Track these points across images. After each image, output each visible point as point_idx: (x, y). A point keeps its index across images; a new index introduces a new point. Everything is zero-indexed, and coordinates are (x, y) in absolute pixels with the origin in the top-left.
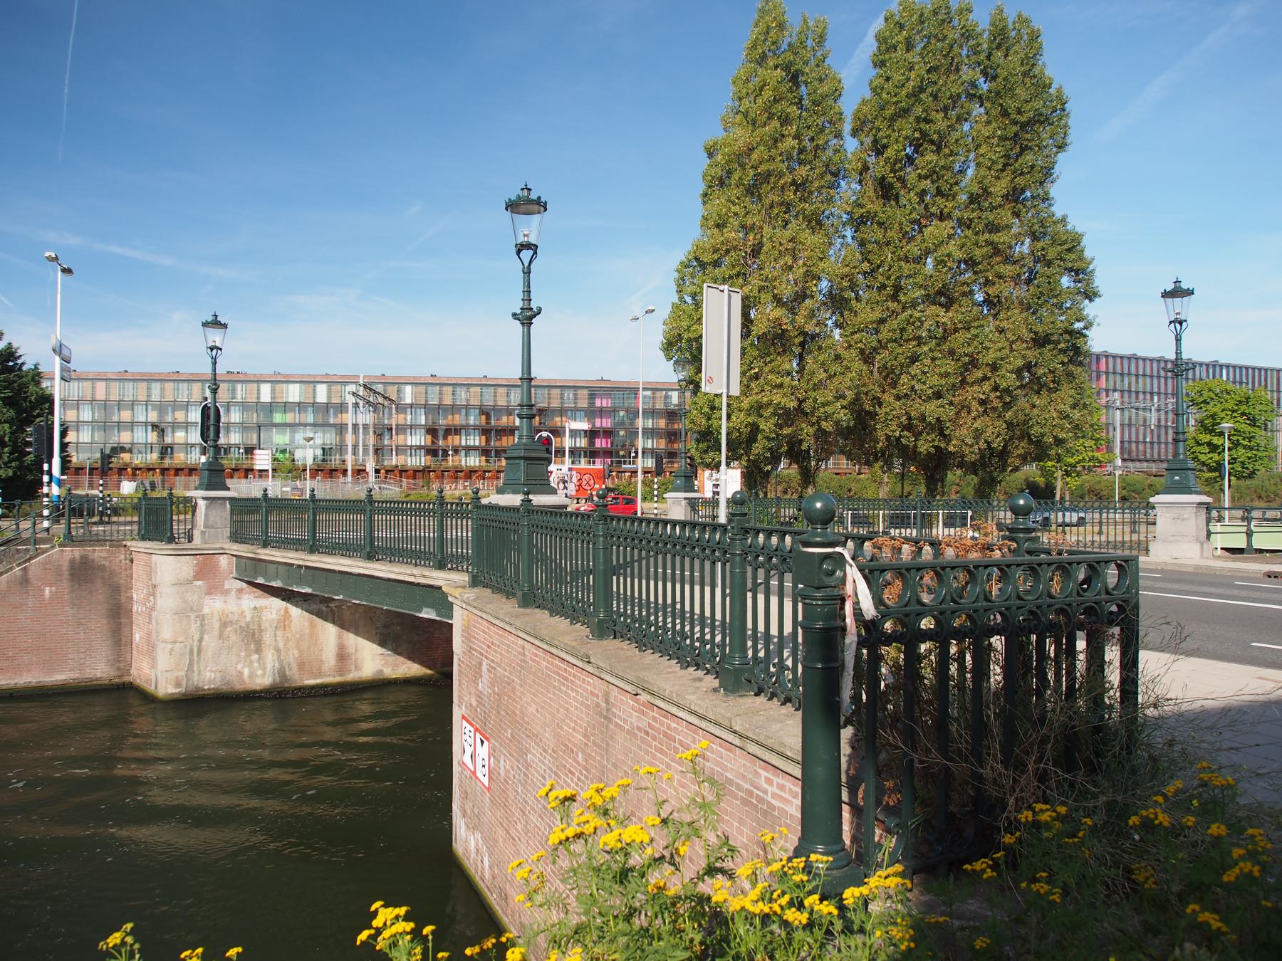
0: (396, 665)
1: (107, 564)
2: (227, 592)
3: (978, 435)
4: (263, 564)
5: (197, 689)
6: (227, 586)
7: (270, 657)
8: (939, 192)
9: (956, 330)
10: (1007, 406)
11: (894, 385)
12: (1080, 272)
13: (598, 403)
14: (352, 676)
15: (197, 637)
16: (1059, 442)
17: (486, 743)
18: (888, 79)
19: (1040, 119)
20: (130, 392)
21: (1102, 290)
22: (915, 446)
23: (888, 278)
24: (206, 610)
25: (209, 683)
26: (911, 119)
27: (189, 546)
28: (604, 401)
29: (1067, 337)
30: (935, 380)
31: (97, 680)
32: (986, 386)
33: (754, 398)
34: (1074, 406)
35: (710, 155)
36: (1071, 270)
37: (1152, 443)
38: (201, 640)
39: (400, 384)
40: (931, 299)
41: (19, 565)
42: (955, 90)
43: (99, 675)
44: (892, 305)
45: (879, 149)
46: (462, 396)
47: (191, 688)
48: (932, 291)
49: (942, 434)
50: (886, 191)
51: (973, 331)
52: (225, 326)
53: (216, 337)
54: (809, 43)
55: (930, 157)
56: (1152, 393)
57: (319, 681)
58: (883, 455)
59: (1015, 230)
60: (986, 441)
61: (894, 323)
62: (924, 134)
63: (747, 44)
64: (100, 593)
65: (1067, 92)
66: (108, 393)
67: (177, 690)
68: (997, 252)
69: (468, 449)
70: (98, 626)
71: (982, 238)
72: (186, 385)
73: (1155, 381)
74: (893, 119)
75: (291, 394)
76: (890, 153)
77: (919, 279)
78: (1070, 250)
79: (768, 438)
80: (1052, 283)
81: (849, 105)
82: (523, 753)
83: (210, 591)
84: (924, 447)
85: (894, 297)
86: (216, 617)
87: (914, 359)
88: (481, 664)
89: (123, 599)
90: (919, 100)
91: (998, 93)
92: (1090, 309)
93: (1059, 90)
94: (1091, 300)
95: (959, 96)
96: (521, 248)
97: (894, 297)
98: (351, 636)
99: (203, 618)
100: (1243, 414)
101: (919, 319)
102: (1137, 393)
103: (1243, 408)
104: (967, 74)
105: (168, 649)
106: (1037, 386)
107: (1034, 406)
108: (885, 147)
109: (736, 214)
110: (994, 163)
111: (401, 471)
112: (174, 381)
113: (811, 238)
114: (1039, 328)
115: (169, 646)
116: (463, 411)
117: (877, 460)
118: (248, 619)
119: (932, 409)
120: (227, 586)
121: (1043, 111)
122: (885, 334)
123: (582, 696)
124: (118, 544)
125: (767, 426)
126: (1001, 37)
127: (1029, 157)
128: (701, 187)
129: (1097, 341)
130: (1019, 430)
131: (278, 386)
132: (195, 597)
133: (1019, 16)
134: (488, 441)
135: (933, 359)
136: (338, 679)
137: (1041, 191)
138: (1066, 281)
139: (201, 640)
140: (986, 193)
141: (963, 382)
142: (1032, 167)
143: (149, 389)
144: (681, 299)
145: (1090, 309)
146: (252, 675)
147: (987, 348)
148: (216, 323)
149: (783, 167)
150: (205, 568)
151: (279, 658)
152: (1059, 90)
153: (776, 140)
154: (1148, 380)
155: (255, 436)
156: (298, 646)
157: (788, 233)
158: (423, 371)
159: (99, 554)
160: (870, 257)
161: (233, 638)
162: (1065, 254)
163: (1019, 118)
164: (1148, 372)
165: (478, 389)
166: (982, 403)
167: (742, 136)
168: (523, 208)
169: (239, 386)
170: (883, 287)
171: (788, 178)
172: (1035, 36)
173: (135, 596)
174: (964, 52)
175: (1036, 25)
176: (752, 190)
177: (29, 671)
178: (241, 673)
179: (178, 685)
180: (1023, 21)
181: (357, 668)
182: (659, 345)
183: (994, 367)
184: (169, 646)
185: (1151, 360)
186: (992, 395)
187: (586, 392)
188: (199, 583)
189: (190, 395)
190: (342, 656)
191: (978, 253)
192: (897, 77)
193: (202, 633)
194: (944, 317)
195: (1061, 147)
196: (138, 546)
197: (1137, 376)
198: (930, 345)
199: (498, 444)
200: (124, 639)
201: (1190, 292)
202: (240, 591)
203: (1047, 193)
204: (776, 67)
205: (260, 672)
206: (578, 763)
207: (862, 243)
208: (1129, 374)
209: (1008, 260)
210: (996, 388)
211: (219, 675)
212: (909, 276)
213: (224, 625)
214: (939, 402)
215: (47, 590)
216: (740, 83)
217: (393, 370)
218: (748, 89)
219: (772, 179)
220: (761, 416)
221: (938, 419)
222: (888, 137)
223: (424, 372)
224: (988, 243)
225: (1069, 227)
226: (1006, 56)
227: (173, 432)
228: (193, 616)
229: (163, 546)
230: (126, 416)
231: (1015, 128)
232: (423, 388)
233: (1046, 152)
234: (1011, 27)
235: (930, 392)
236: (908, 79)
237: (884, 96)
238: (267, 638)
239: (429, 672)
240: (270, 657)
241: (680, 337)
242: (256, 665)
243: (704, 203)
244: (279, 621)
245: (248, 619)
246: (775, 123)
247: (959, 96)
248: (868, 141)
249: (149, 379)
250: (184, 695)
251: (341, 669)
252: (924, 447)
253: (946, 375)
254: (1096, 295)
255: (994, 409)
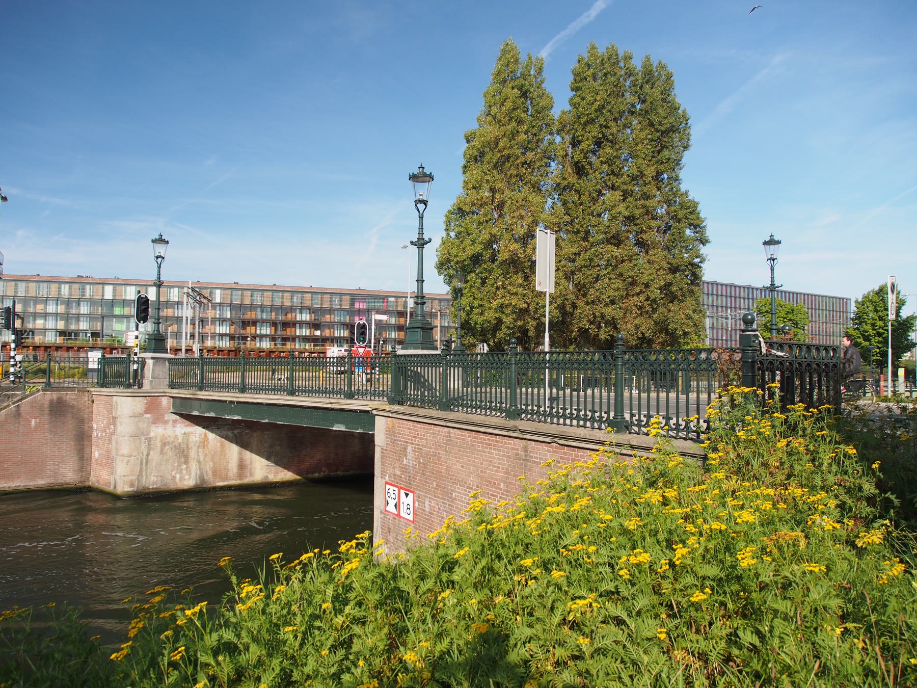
0: (277, 473)
1: (76, 403)
2: (166, 422)
3: (637, 328)
4: (189, 401)
5: (145, 488)
6: (166, 418)
7: (194, 466)
8: (613, 173)
9: (623, 261)
10: (654, 310)
11: (584, 295)
12: (697, 226)
13: (357, 305)
14: (247, 480)
15: (145, 453)
16: (685, 334)
17: (411, 495)
18: (583, 99)
19: (673, 130)
20: (44, 291)
21: (711, 239)
22: (598, 335)
23: (582, 226)
24: (152, 434)
25: (153, 484)
26: (597, 126)
27: (140, 390)
28: (361, 304)
29: (690, 267)
30: (612, 293)
31: (67, 484)
32: (642, 297)
33: (500, 301)
34: (694, 311)
35: (468, 141)
36: (691, 225)
37: (726, 340)
38: (148, 455)
39: (212, 288)
40: (608, 241)
41: (14, 403)
42: (622, 108)
43: (68, 481)
44: (585, 244)
45: (575, 143)
46: (258, 299)
47: (140, 488)
48: (609, 236)
49: (615, 328)
50: (580, 170)
51: (633, 262)
52: (167, 242)
53: (160, 249)
54: (532, 72)
55: (608, 150)
56: (726, 307)
57: (226, 483)
58: (576, 340)
59: (658, 198)
60: (643, 334)
61: (585, 255)
62: (604, 136)
63: (494, 71)
64: (70, 424)
65: (689, 113)
66: (27, 291)
67: (131, 489)
68: (647, 213)
69: (262, 337)
70: (68, 448)
71: (639, 203)
72: (45, 285)
73: (729, 299)
74: (585, 124)
75: (128, 293)
76: (583, 146)
77: (602, 228)
78: (691, 213)
79: (508, 328)
80: (681, 233)
81: (556, 113)
82: (448, 494)
83: (156, 421)
84: (603, 336)
85: (585, 239)
86: (159, 439)
87: (597, 279)
88: (405, 449)
89: (86, 428)
90: (602, 113)
91: (647, 112)
92: (703, 250)
93: (684, 111)
94: (704, 245)
95: (624, 112)
96: (418, 202)
97: (585, 239)
98: (248, 452)
99: (150, 439)
100: (790, 320)
101: (601, 253)
102: (717, 307)
103: (790, 316)
104: (629, 98)
105: (125, 461)
106: (672, 298)
107: (669, 311)
108: (580, 142)
109: (488, 181)
110: (646, 155)
111: (219, 351)
112: (37, 281)
113: (535, 199)
114: (674, 262)
115: (126, 459)
116: (259, 310)
117: (571, 344)
118: (180, 441)
119: (609, 311)
120: (166, 418)
121: (674, 123)
122: (579, 262)
123: (503, 451)
124: (83, 391)
125: (507, 320)
126: (649, 76)
127: (666, 153)
128: (463, 162)
129: (709, 273)
130: (663, 327)
131: (118, 288)
132: (145, 425)
133: (660, 63)
134: (276, 330)
135: (610, 279)
136: (238, 482)
137: (674, 175)
138: (688, 232)
139: (148, 455)
140: (642, 175)
141: (628, 295)
142: (669, 159)
143: (16, 287)
144: (448, 234)
145: (703, 250)
146: (182, 479)
147: (642, 273)
148: (161, 240)
149: (518, 152)
150: (152, 407)
151: (200, 467)
152: (684, 111)
153: (514, 134)
154: (724, 298)
155: (99, 324)
156: (212, 460)
157: (522, 195)
158: (229, 279)
159: (70, 397)
160: (570, 212)
161: (170, 453)
162: (687, 216)
163: (660, 128)
164: (724, 293)
165: (270, 293)
166: (640, 308)
167: (492, 131)
168: (421, 179)
169: (88, 287)
170: (578, 232)
171: (522, 159)
172: (669, 77)
173: (95, 426)
174: (628, 83)
175: (670, 69)
176: (498, 166)
177: (19, 478)
178: (174, 478)
179: (132, 485)
180: (662, 66)
181: (251, 475)
182: (434, 264)
183: (647, 286)
184: (126, 459)
185: (726, 285)
186: (646, 303)
187: (348, 297)
188: (148, 416)
189: (49, 292)
190: (242, 466)
191: (637, 212)
192: (589, 98)
193: (149, 449)
194: (617, 252)
195: (686, 147)
196: (96, 390)
197: (717, 295)
198: (608, 270)
199: (284, 333)
200: (86, 456)
201: (779, 242)
202: (175, 421)
203: (677, 176)
204: (513, 88)
205: (187, 477)
206: (501, 489)
207: (565, 203)
208: (712, 294)
209: (654, 218)
210: (647, 299)
211: (159, 479)
212: (594, 226)
213: (164, 444)
214: (613, 307)
215: (33, 422)
216: (489, 97)
217: (206, 278)
218: (494, 101)
219: (512, 159)
220: (503, 313)
221: (613, 318)
222: (583, 136)
223: (229, 280)
224: (644, 206)
225: (690, 198)
226: (652, 88)
227: (35, 320)
228: (143, 438)
229: (122, 390)
230: (40, 308)
231: (658, 134)
232: (229, 292)
233: (677, 150)
234: (655, 69)
235: (608, 300)
236: (596, 100)
237: (581, 109)
238: (192, 454)
239: (298, 477)
240: (194, 466)
241: (449, 260)
242: (184, 472)
243: (464, 172)
244: (200, 442)
245: (180, 441)
246: (514, 124)
247: (624, 112)
248: (568, 138)
249: (60, 282)
250: (136, 492)
251: (241, 475)
252: (603, 336)
253: (618, 289)
254: (707, 241)
255: (647, 312)
